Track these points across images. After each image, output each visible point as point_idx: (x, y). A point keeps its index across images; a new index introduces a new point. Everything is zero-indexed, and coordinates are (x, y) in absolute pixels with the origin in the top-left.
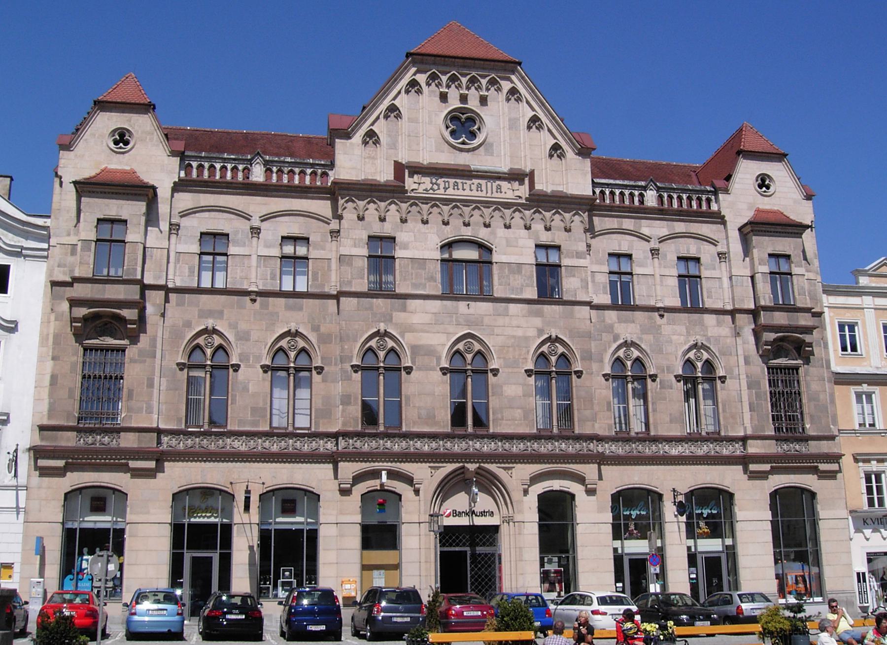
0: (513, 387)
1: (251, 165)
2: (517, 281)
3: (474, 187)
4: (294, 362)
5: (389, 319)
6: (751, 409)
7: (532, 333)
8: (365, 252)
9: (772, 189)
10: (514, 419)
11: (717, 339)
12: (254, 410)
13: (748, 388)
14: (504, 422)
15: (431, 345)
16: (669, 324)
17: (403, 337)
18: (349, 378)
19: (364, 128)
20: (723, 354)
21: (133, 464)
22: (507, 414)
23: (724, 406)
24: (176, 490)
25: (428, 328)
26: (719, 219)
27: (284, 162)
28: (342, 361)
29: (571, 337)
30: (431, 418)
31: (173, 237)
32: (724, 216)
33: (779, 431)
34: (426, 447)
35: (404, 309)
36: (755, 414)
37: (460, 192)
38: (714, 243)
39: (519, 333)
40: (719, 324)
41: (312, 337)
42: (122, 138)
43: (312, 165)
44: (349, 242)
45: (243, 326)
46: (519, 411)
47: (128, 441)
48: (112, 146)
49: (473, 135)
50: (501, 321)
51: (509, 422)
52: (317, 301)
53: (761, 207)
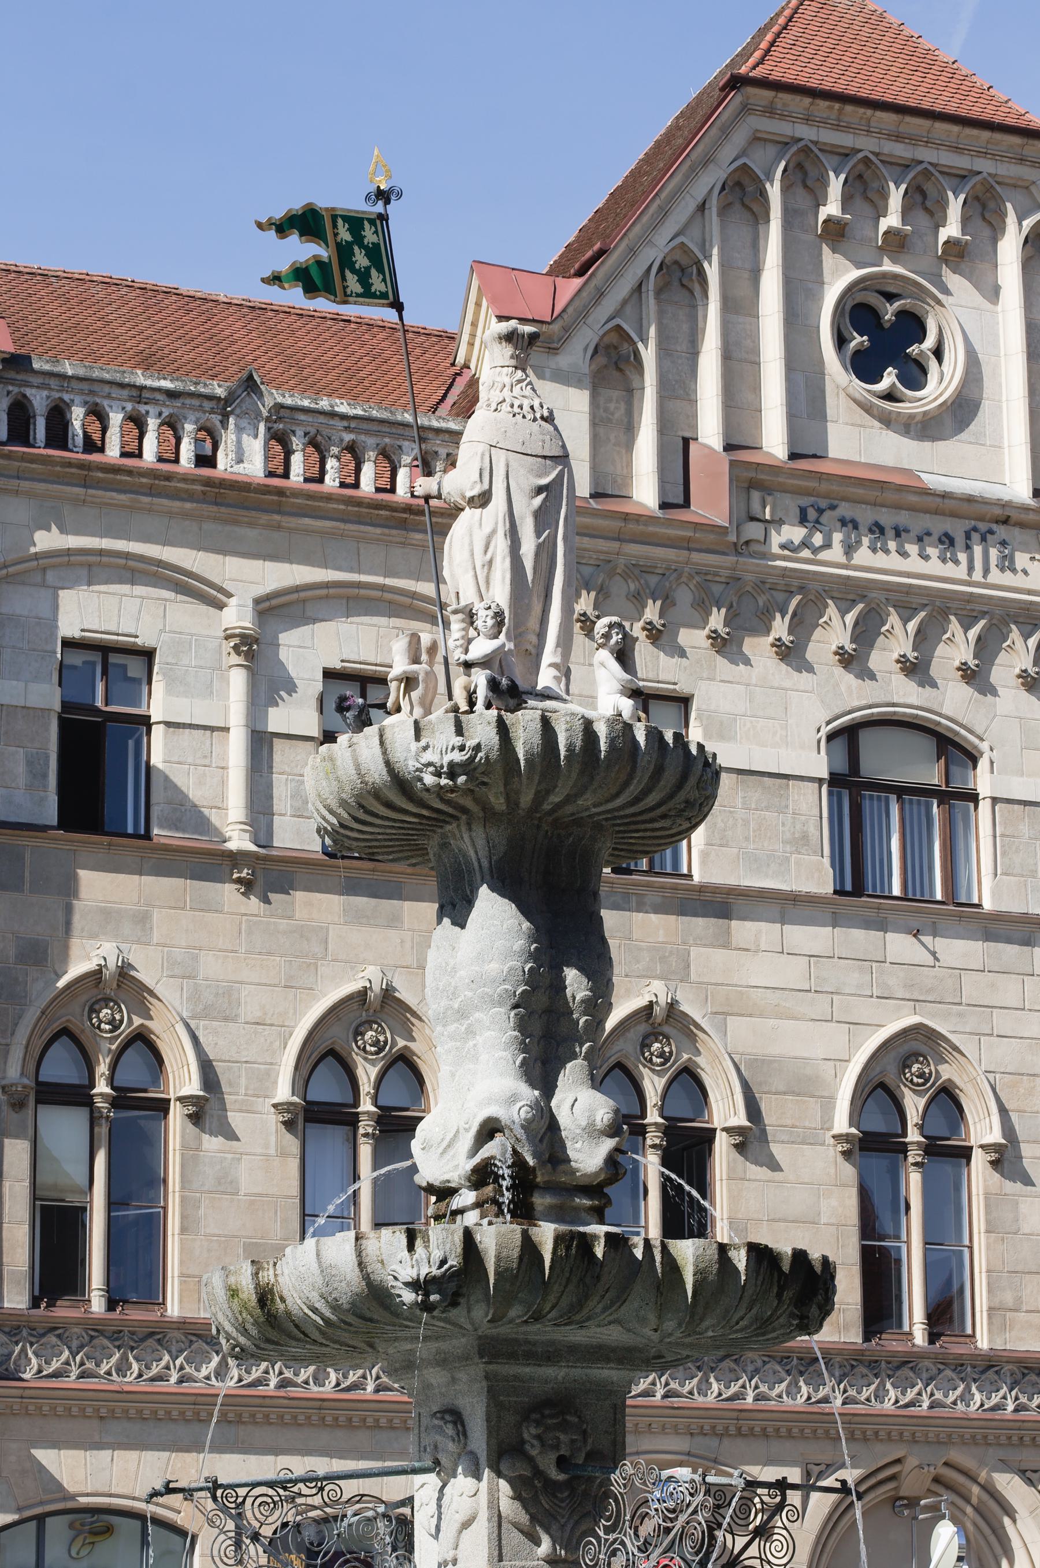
1: (225, 416)
5: (679, 970)
27: (332, 414)
45: (210, 966)
49: (914, 375)
50: (1009, 991)
52: (682, 481)
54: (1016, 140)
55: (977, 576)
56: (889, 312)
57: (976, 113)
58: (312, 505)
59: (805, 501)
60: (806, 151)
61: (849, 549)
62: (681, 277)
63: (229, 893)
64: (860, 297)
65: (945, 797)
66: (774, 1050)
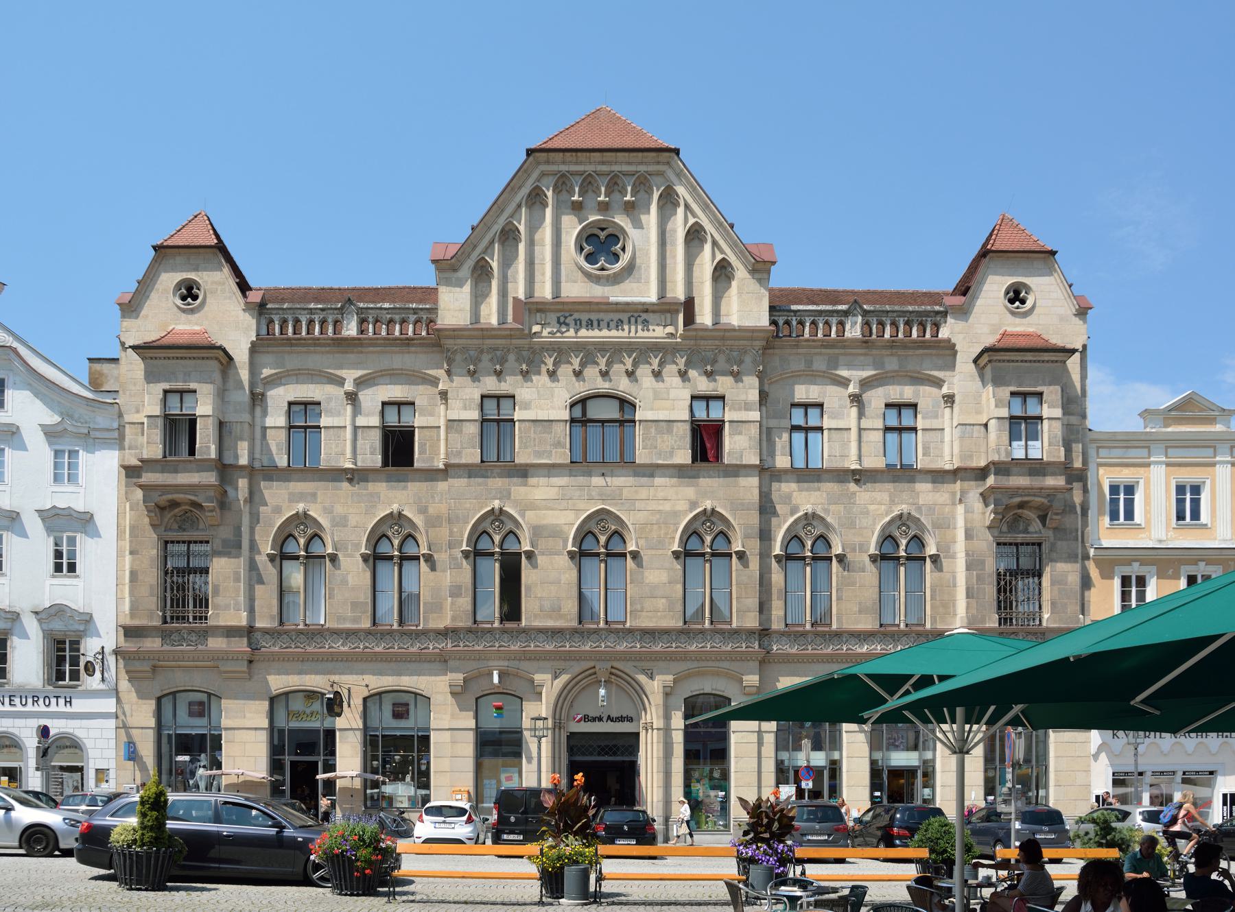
0: (657, 572)
4: (606, 547)
6: (969, 595)
7: (682, 506)
8: (475, 414)
9: (1029, 304)
11: (931, 509)
12: (355, 605)
13: (967, 569)
15: (557, 525)
17: (523, 516)
18: (460, 567)
20: (937, 526)
22: (648, 604)
23: (933, 591)
25: (551, 509)
26: (949, 349)
27: (381, 308)
28: (451, 546)
29: (733, 510)
30: (556, 611)
31: (258, 410)
32: (954, 345)
33: (1005, 623)
36: (973, 601)
37: (596, 333)
38: (938, 383)
39: (667, 507)
41: (418, 520)
42: (189, 292)
43: (415, 311)
45: (339, 509)
46: (664, 600)
48: (179, 302)
50: (643, 493)
51: (650, 614)
53: (1010, 329)
54: (653, 154)
55: (632, 334)
56: (602, 235)
57: (647, 145)
58: (373, 342)
59: (559, 314)
60: (563, 176)
61: (577, 331)
62: (509, 236)
63: (345, 485)
64: (590, 232)
65: (622, 423)
66: (544, 522)
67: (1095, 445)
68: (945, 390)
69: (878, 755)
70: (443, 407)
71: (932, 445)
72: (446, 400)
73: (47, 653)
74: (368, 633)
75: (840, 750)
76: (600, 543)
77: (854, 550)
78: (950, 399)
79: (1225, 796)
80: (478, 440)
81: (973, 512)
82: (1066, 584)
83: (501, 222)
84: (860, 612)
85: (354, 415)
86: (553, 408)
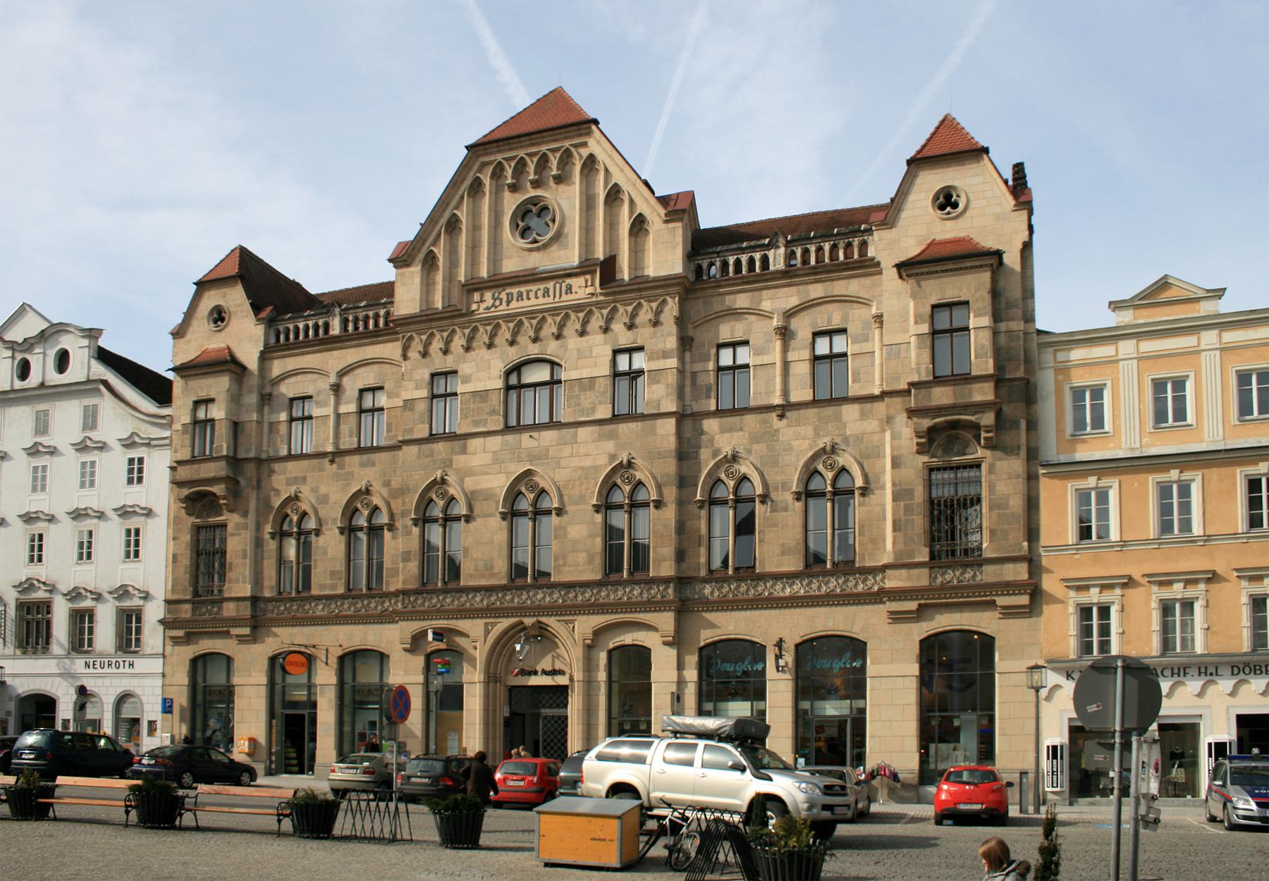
0: (578, 527)
2: (587, 399)
3: (540, 294)
5: (448, 463)
6: (896, 528)
9: (961, 206)
10: (577, 565)
14: (566, 569)
16: (788, 426)
18: (409, 533)
19: (424, 251)
21: (1001, 601)
23: (862, 527)
24: (799, 640)
25: (486, 469)
31: (266, 409)
34: (478, 600)
35: (464, 451)
37: (526, 303)
39: (588, 462)
40: (864, 416)
42: (219, 316)
44: (411, 385)
45: (323, 490)
46: (584, 555)
47: (989, 574)
50: (567, 451)
66: (480, 487)
67: (1051, 350)
68: (874, 311)
69: (805, 705)
70: (877, 332)
71: (862, 371)
72: (881, 323)
73: (119, 624)
74: (342, 597)
75: (864, 698)
76: (525, 503)
77: (776, 489)
78: (879, 318)
79: (1210, 745)
80: (426, 416)
81: (900, 438)
82: (1007, 508)
83: (447, 215)
84: (783, 554)
85: (337, 404)
86: (489, 378)
